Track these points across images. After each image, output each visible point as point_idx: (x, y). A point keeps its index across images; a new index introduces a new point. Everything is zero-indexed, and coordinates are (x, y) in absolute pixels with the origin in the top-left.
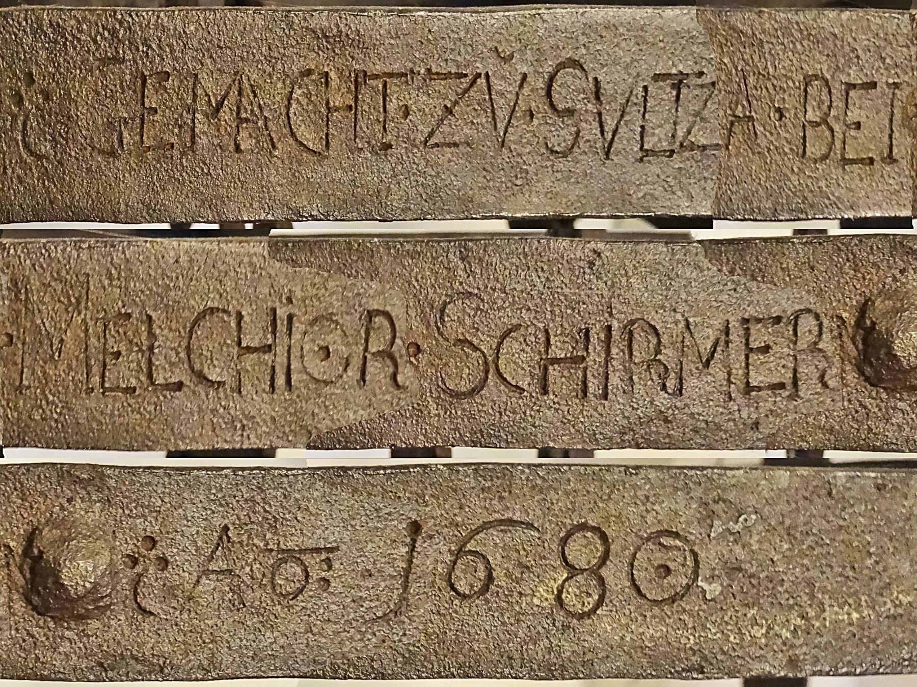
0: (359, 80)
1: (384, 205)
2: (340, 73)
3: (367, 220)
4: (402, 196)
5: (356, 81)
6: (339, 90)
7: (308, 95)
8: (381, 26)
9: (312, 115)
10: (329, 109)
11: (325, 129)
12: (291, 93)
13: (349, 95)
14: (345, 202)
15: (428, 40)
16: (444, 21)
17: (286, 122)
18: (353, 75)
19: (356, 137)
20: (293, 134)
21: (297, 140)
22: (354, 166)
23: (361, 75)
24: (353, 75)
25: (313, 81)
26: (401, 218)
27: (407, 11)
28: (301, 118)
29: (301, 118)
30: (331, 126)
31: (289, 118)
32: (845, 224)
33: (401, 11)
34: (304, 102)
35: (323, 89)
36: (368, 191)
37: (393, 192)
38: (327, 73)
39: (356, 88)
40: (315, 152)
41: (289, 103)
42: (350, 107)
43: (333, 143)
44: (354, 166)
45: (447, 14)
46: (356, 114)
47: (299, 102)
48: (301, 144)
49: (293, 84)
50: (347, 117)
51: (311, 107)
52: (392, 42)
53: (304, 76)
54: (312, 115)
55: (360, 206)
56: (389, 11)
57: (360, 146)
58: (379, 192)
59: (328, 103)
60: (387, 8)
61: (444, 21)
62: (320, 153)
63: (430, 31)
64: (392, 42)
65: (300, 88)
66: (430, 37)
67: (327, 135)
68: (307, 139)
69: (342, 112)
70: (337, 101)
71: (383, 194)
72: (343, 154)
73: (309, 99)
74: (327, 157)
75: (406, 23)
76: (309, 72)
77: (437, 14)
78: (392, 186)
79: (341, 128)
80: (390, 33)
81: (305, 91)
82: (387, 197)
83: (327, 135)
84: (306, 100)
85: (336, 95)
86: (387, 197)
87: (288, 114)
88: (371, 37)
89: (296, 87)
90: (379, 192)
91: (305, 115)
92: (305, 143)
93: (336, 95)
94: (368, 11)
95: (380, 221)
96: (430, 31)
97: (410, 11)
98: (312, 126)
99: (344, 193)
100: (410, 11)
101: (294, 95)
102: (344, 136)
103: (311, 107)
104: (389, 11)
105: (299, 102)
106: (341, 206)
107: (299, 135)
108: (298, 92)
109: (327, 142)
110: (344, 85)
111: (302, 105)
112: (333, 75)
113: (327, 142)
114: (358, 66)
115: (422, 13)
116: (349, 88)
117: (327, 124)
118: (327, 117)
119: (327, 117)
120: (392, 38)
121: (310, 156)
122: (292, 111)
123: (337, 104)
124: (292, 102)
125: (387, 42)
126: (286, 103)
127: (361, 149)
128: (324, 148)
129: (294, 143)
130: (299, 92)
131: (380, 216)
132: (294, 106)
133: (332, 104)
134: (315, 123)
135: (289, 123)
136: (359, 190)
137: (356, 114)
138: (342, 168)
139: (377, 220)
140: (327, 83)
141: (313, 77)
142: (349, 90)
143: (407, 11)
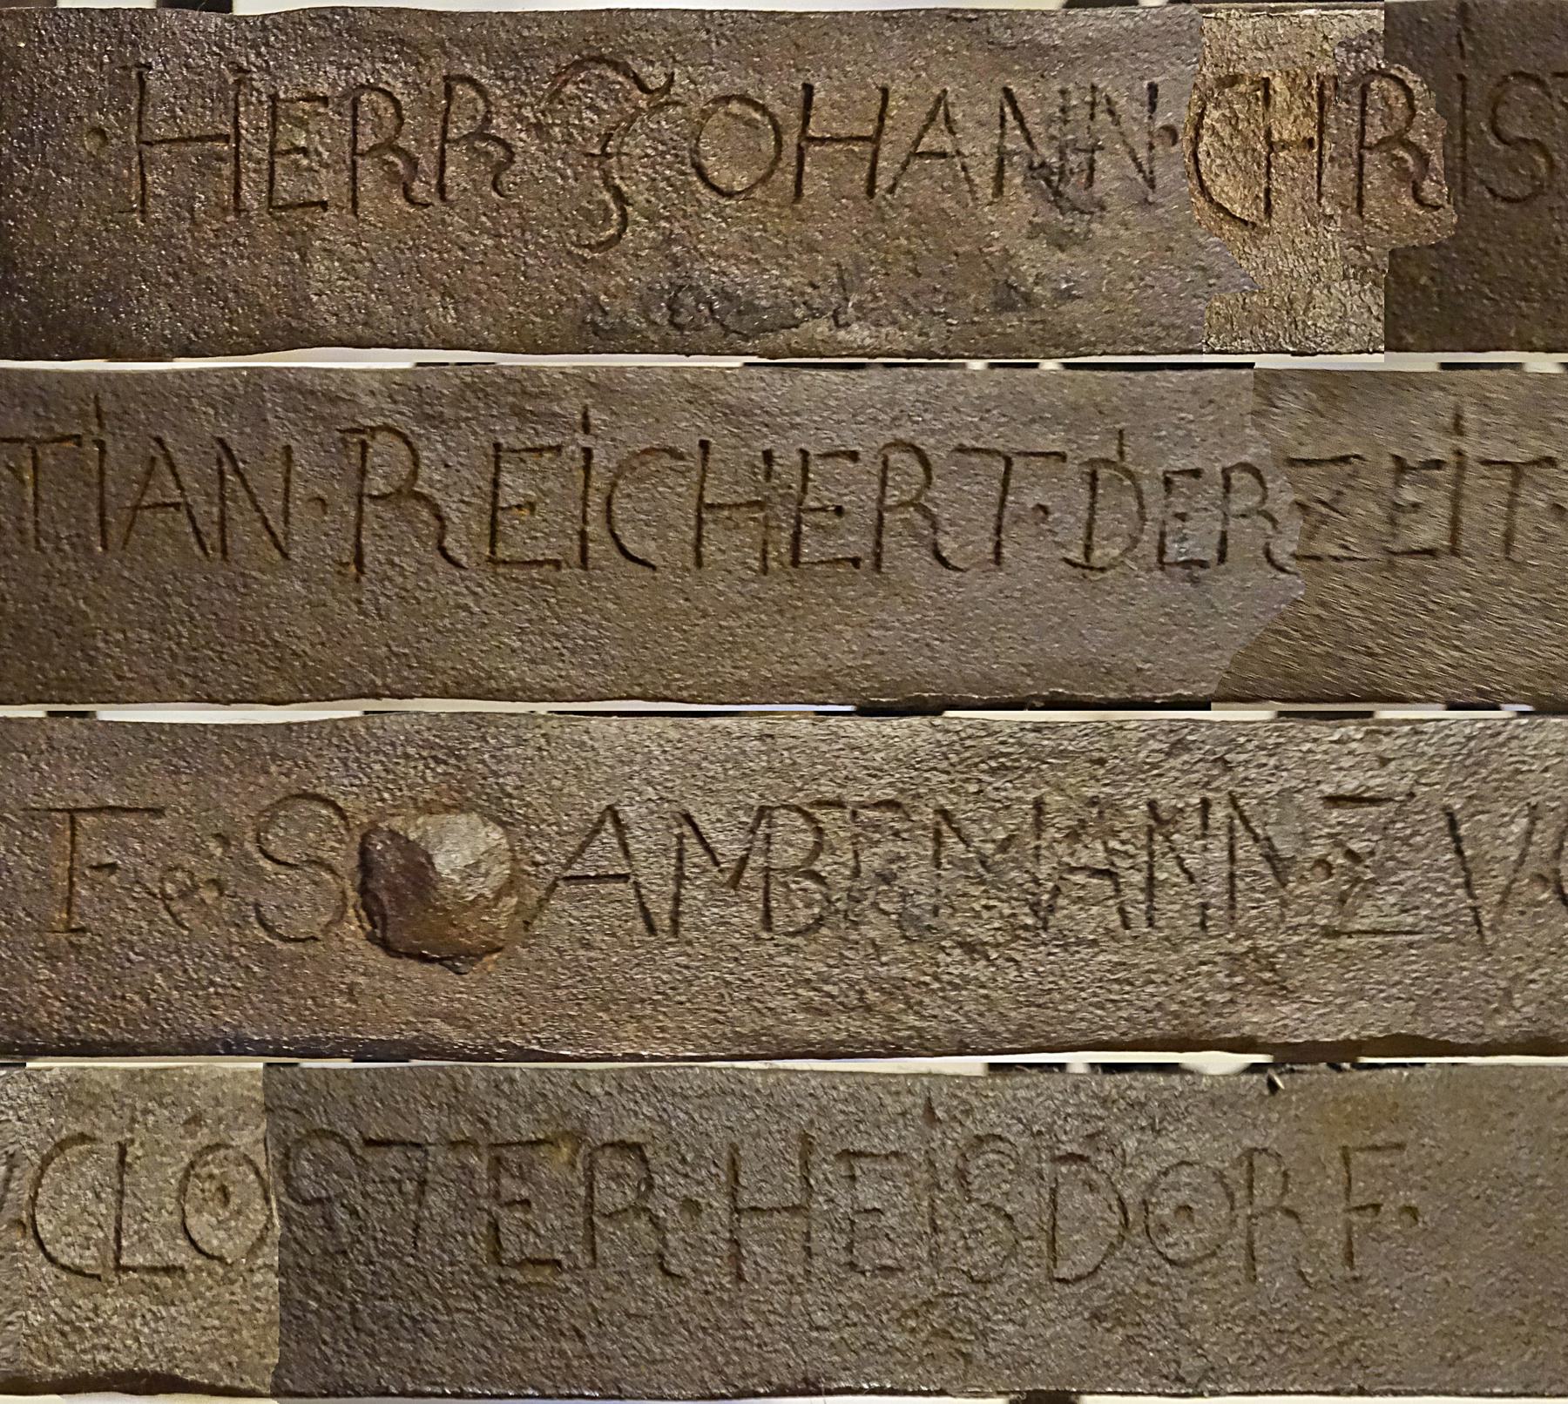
0: (1327, 93)
1: (1300, 326)
2: (1292, 81)
3: (1269, 352)
4: (1334, 310)
5: (1321, 94)
6: (1290, 111)
7: (1232, 121)
8: (1239, 33)
9: (1240, 157)
10: (1271, 145)
11: (1263, 181)
12: (1201, 116)
13: (1308, 120)
14: (1229, 319)
15: (1324, 52)
16: (1351, 23)
17: (1192, 168)
18: (1315, 85)
19: (1320, 195)
20: (1204, 190)
21: (1211, 201)
22: (1317, 248)
23: (1330, 84)
24: (1315, 85)
25: (1242, 95)
26: (1331, 349)
27: (1285, 9)
28: (1219, 161)
29: (1219, 161)
30: (1274, 176)
31: (1197, 161)
32: (1035, 365)
33: (1275, 10)
34: (1225, 132)
35: (1260, 110)
36: (1271, 301)
37: (1317, 302)
38: (1267, 80)
39: (1321, 108)
40: (1246, 223)
41: (1198, 135)
42: (1310, 142)
43: (1279, 206)
44: (1317, 248)
45: (1354, 12)
46: (1320, 154)
47: (1215, 132)
48: (1220, 208)
49: (1204, 101)
50: (1305, 160)
51: (1237, 142)
52: (1260, 55)
53: (1225, 86)
54: (1240, 157)
55: (1256, 328)
56: (1253, 10)
57: (1328, 211)
58: (1291, 302)
59: (1268, 134)
60: (1249, 5)
61: (1351, 23)
62: (1254, 225)
63: (1325, 37)
64: (1260, 55)
65: (1217, 107)
66: (1326, 46)
67: (1268, 191)
68: (1230, 200)
69: (1294, 151)
70: (1285, 130)
71: (1300, 306)
72: (1297, 226)
73: (1235, 128)
74: (1267, 232)
75: (1284, 26)
76: (1234, 80)
77: (1337, 12)
78: (1316, 292)
79: (1293, 179)
80: (1255, 42)
81: (1227, 112)
82: (1306, 311)
83: (1268, 191)
84: (1228, 129)
85: (1285, 121)
86: (1306, 311)
87: (1195, 154)
88: (1222, 49)
89: (1210, 106)
90: (1291, 302)
91: (1227, 155)
92: (1228, 206)
93: (1285, 121)
94: (1215, 10)
95: (1293, 354)
96: (1325, 37)
97: (1290, 9)
98: (1240, 176)
99: (1228, 304)
100: (1290, 9)
101: (1207, 120)
102: (1298, 192)
103: (1237, 142)
104: (1253, 10)
105: (1215, 132)
106: (1222, 326)
107: (1215, 191)
108: (1213, 115)
109: (1268, 205)
110: (1299, 103)
111: (1221, 139)
112: (1277, 84)
113: (1268, 205)
114: (1324, 69)
115: (1312, 12)
116: (1308, 107)
117: (1268, 173)
118: (1268, 159)
119: (1268, 159)
120: (1259, 49)
121: (1236, 230)
122: (1202, 148)
123: (1286, 136)
124: (1203, 132)
125: (1250, 55)
126: (1192, 134)
127: (1331, 217)
128: (1262, 216)
129: (1206, 206)
130: (1216, 114)
131: (1294, 345)
132: (1206, 139)
133: (1276, 136)
134: (1245, 171)
135: (1198, 171)
136: (1255, 298)
137: (1320, 154)
138: (1296, 251)
139: (1287, 352)
140: (1267, 99)
141: (1242, 88)
142: (1308, 111)
143: (1285, 9)
